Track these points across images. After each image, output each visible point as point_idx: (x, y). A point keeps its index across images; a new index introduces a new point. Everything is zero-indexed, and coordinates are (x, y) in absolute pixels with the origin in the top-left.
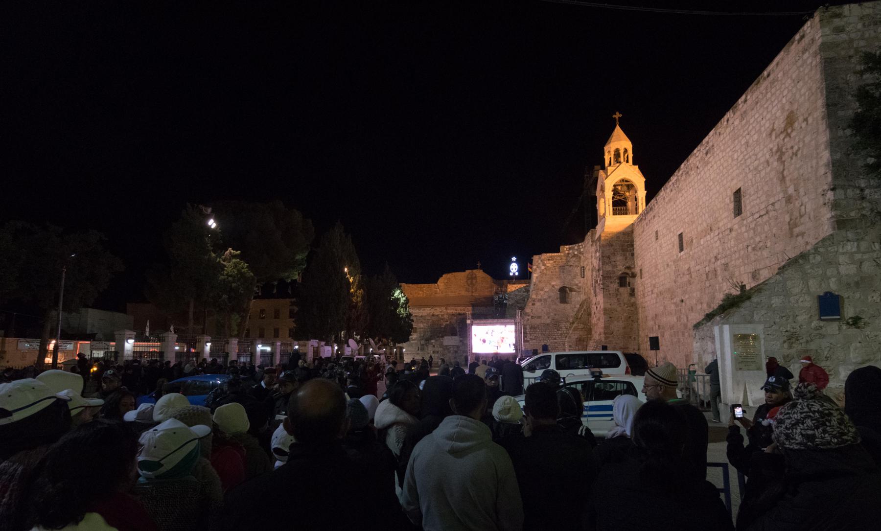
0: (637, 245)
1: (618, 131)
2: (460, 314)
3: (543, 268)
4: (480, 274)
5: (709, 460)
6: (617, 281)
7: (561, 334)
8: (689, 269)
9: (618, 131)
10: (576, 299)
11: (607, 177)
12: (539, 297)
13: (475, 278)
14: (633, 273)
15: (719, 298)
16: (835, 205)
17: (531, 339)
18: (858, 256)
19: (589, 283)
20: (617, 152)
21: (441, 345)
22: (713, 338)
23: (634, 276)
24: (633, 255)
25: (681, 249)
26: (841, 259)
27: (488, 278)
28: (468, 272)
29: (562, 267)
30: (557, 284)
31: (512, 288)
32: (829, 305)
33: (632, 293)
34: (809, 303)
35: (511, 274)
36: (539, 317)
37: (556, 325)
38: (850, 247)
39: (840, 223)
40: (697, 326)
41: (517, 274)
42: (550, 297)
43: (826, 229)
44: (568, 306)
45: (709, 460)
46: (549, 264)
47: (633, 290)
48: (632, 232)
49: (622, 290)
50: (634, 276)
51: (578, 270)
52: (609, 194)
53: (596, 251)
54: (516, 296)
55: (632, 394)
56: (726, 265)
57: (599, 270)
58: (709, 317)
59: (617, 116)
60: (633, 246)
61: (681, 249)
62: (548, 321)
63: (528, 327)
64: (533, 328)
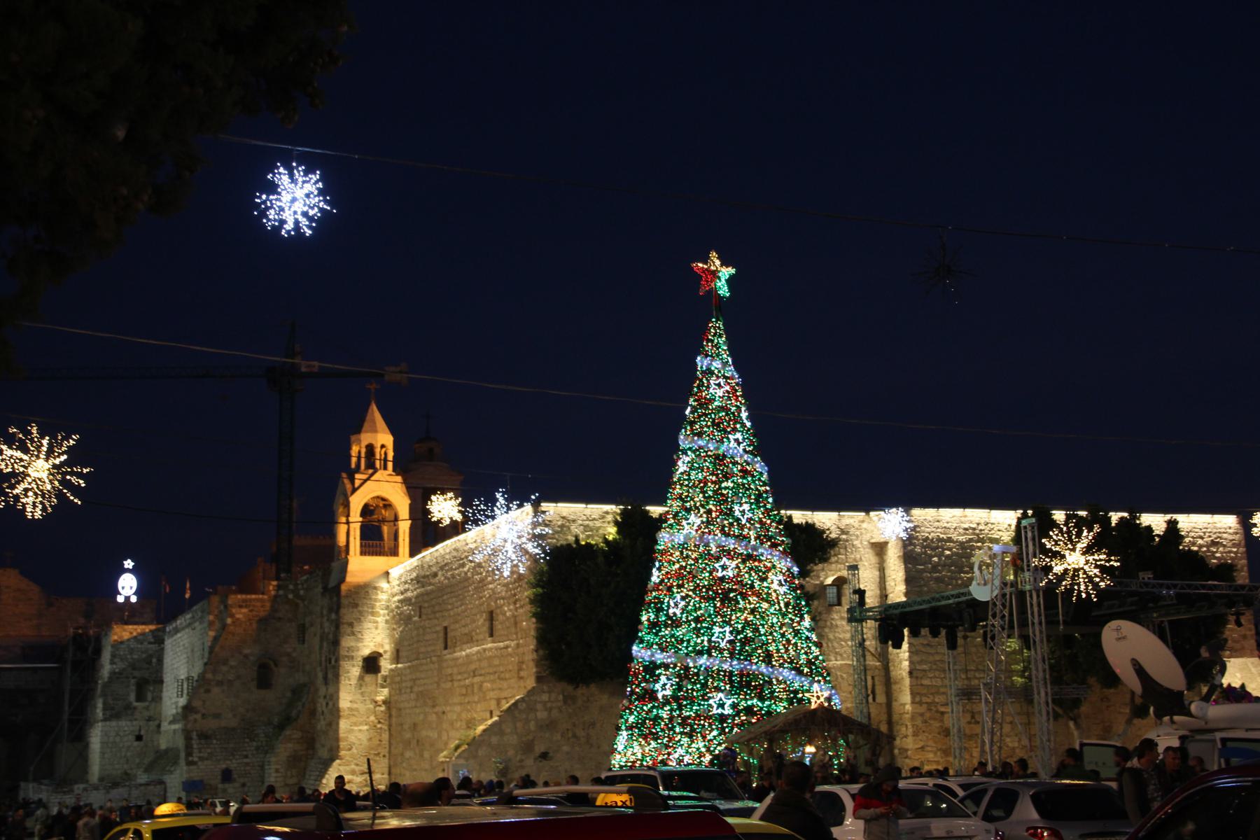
1: (375, 414)
7: (257, 748)
11: (354, 490)
12: (219, 677)
17: (201, 759)
18: (549, 705)
20: (370, 449)
26: (539, 706)
31: (123, 633)
35: (120, 599)
36: (217, 716)
38: (545, 697)
41: (134, 599)
52: (355, 516)
54: (132, 651)
63: (194, 735)
64: (205, 736)
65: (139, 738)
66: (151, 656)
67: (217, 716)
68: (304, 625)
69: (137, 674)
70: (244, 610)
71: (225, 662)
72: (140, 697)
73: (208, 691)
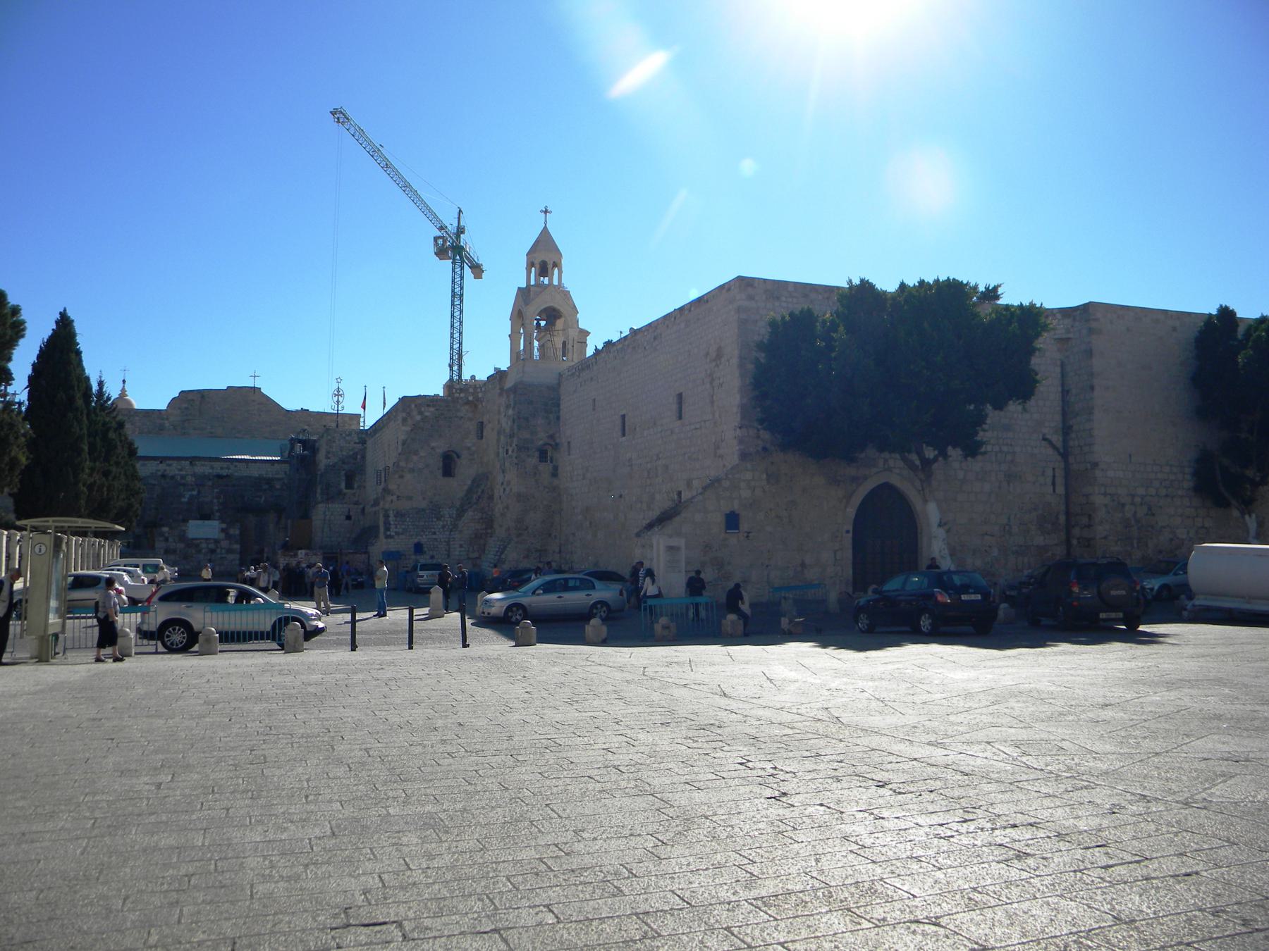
2: (219, 476)
3: (418, 418)
6: (537, 454)
7: (443, 527)
8: (630, 460)
10: (466, 471)
12: (411, 465)
14: (557, 445)
16: (741, 442)
21: (182, 538)
22: (652, 546)
24: (558, 418)
25: (624, 435)
32: (732, 521)
33: (555, 474)
34: (719, 519)
36: (410, 498)
38: (748, 476)
39: (744, 456)
40: (638, 535)
42: (427, 466)
43: (735, 459)
47: (556, 468)
48: (559, 384)
49: (542, 467)
53: (508, 407)
56: (666, 467)
57: (512, 436)
58: (650, 526)
60: (559, 405)
61: (624, 435)
62: (424, 504)
63: (391, 514)
65: (348, 518)
66: (356, 454)
67: (410, 498)
68: (482, 423)
69: (346, 467)
70: (432, 409)
71: (416, 453)
72: (349, 485)
73: (401, 477)
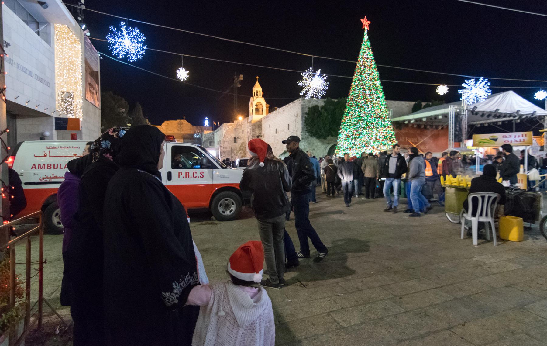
0: (263, 126)
1: (257, 84)
4: (184, 122)
5: (16, 262)
9: (257, 84)
13: (182, 124)
15: (283, 151)
19: (246, 136)
23: (261, 136)
27: (189, 124)
28: (178, 121)
29: (235, 129)
30: (233, 135)
31: (206, 132)
37: (232, 151)
44: (237, 144)
45: (25, 265)
46: (230, 127)
50: (261, 136)
51: (241, 131)
52: (254, 107)
55: (9, 101)
59: (257, 78)
64: (224, 152)
